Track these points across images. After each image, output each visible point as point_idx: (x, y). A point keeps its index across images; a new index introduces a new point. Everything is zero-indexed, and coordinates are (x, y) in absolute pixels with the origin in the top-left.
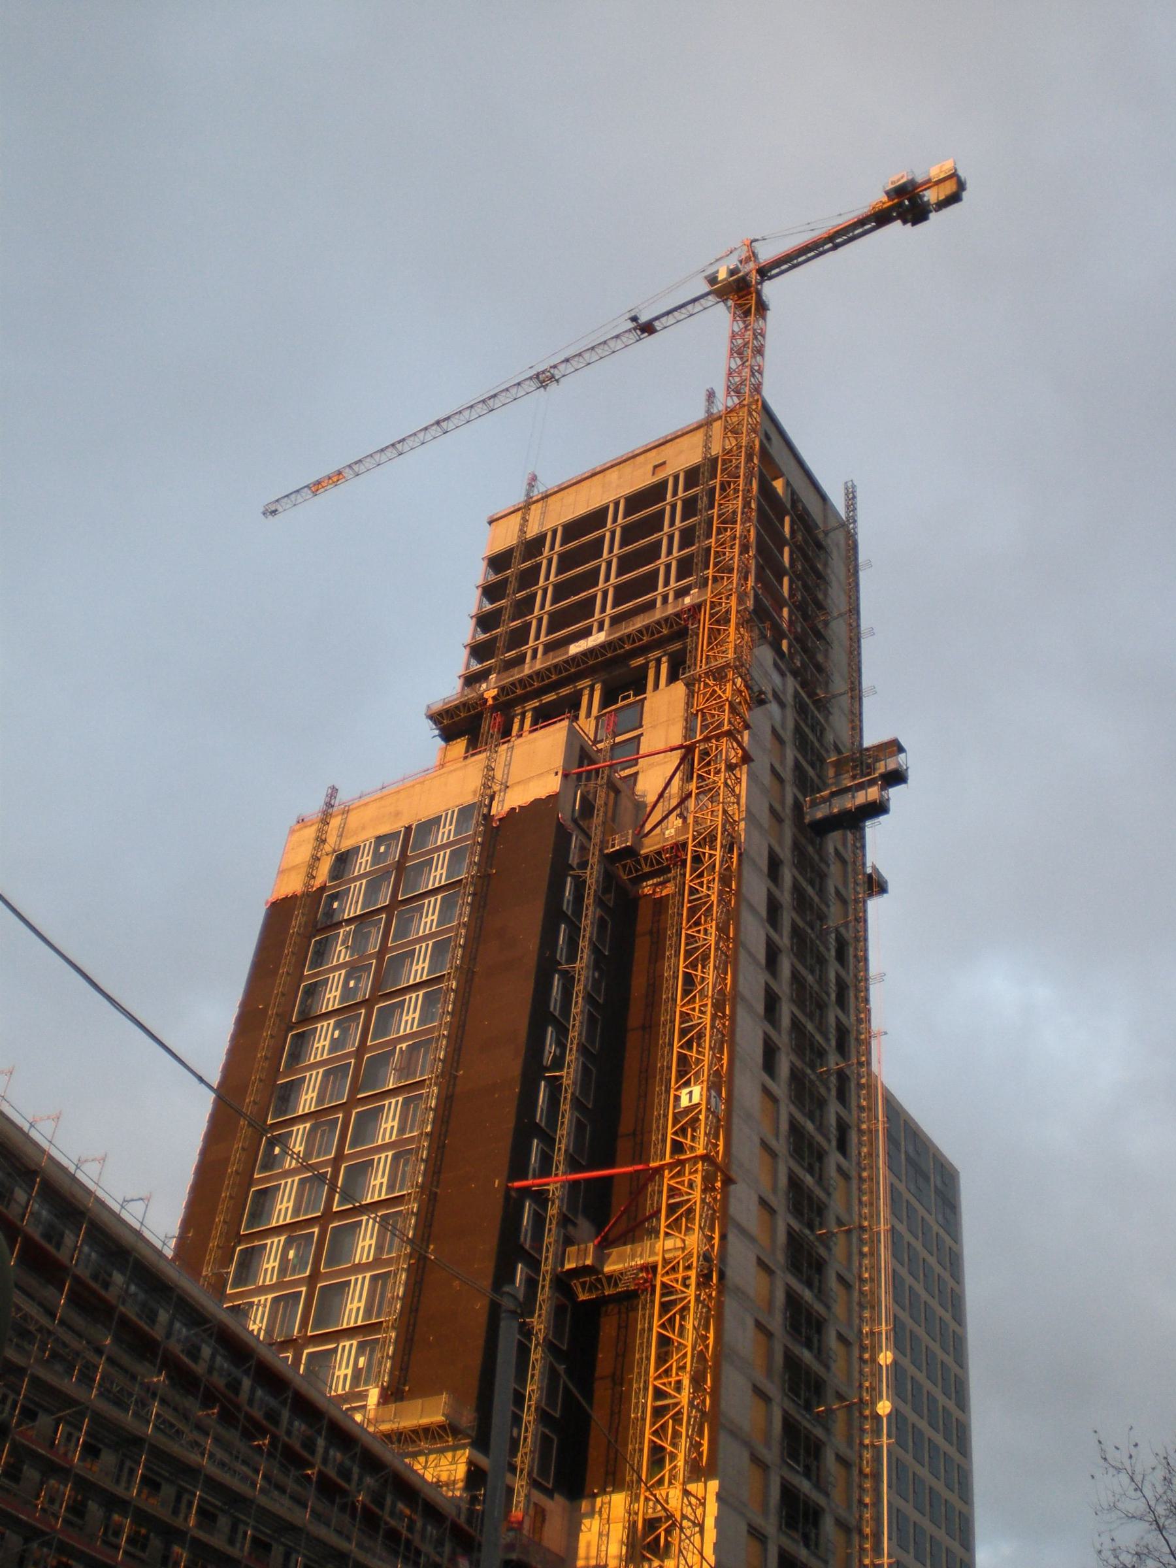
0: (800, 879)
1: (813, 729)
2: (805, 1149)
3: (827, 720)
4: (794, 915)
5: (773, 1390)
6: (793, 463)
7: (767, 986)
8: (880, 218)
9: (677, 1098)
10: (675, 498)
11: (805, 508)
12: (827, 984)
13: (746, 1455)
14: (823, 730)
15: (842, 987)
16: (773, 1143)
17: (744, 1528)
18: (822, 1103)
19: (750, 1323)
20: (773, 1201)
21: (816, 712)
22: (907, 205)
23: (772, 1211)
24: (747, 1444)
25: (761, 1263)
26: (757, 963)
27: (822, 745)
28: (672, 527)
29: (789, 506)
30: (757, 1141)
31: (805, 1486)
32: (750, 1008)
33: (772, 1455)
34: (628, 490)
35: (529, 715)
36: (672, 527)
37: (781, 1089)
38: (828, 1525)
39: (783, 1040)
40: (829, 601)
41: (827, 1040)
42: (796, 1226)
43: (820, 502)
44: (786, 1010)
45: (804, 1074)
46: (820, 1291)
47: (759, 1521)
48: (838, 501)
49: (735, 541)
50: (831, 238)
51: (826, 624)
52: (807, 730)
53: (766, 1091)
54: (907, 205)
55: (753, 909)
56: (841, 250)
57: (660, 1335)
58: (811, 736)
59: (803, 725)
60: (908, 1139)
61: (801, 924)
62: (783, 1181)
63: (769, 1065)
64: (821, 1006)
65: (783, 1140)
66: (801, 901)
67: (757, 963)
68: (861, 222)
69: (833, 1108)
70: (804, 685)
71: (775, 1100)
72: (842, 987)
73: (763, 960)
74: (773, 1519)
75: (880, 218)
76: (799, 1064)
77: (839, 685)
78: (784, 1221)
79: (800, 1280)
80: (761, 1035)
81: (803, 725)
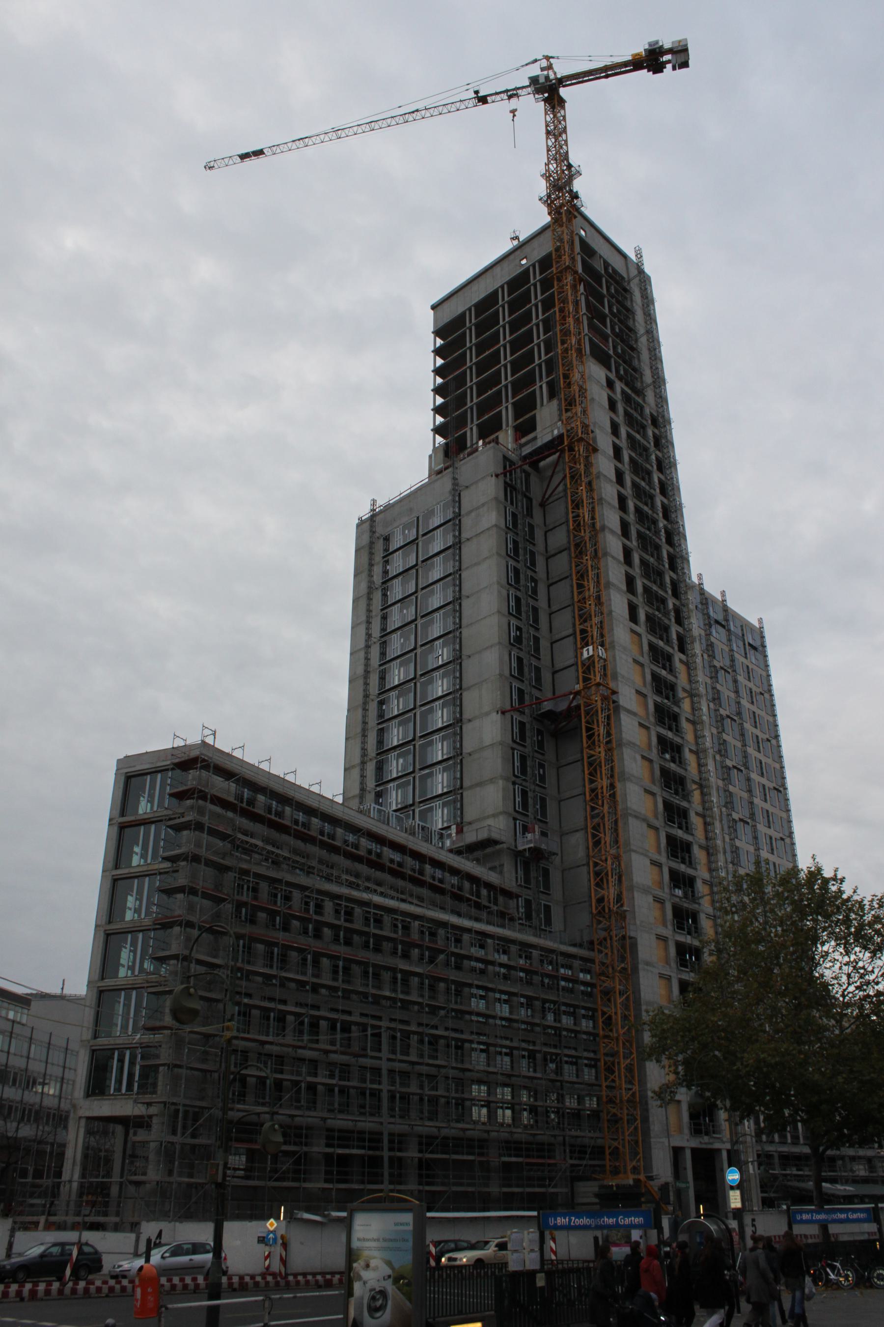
0: (638, 503)
1: (636, 410)
2: (659, 656)
3: (644, 400)
4: (630, 451)
5: (656, 789)
6: (602, 240)
7: (619, 492)
8: (635, 64)
9: (582, 654)
10: (535, 278)
11: (614, 270)
12: (663, 561)
13: (645, 825)
14: (642, 408)
15: (672, 559)
16: (641, 659)
17: (648, 862)
18: (667, 629)
19: (639, 758)
20: (644, 691)
21: (637, 398)
22: (652, 60)
23: (645, 696)
24: (644, 820)
25: (641, 725)
26: (619, 561)
27: (642, 418)
28: (537, 297)
29: (603, 272)
30: (631, 660)
31: (680, 833)
32: (618, 589)
33: (659, 823)
34: (507, 278)
35: (469, 444)
36: (537, 297)
37: (641, 629)
38: (696, 850)
39: (639, 600)
40: (637, 324)
41: (666, 592)
42: (659, 699)
43: (622, 260)
44: (623, 431)
45: (655, 615)
46: (677, 731)
47: (656, 857)
48: (632, 255)
49: (575, 300)
50: (606, 69)
51: (636, 341)
52: (632, 411)
53: (633, 631)
54: (652, 60)
55: (613, 532)
56: (610, 79)
57: (577, 584)
58: (635, 414)
59: (629, 409)
60: (721, 618)
61: (642, 530)
62: (649, 677)
63: (633, 618)
64: (660, 574)
65: (646, 656)
66: (627, 399)
67: (619, 561)
68: (625, 64)
69: (674, 629)
70: (627, 384)
71: (639, 635)
72: (672, 559)
73: (622, 559)
74: (664, 854)
75: (635, 64)
76: (651, 611)
77: (648, 378)
78: (652, 698)
79: (650, 581)
80: (626, 601)
81: (629, 409)
